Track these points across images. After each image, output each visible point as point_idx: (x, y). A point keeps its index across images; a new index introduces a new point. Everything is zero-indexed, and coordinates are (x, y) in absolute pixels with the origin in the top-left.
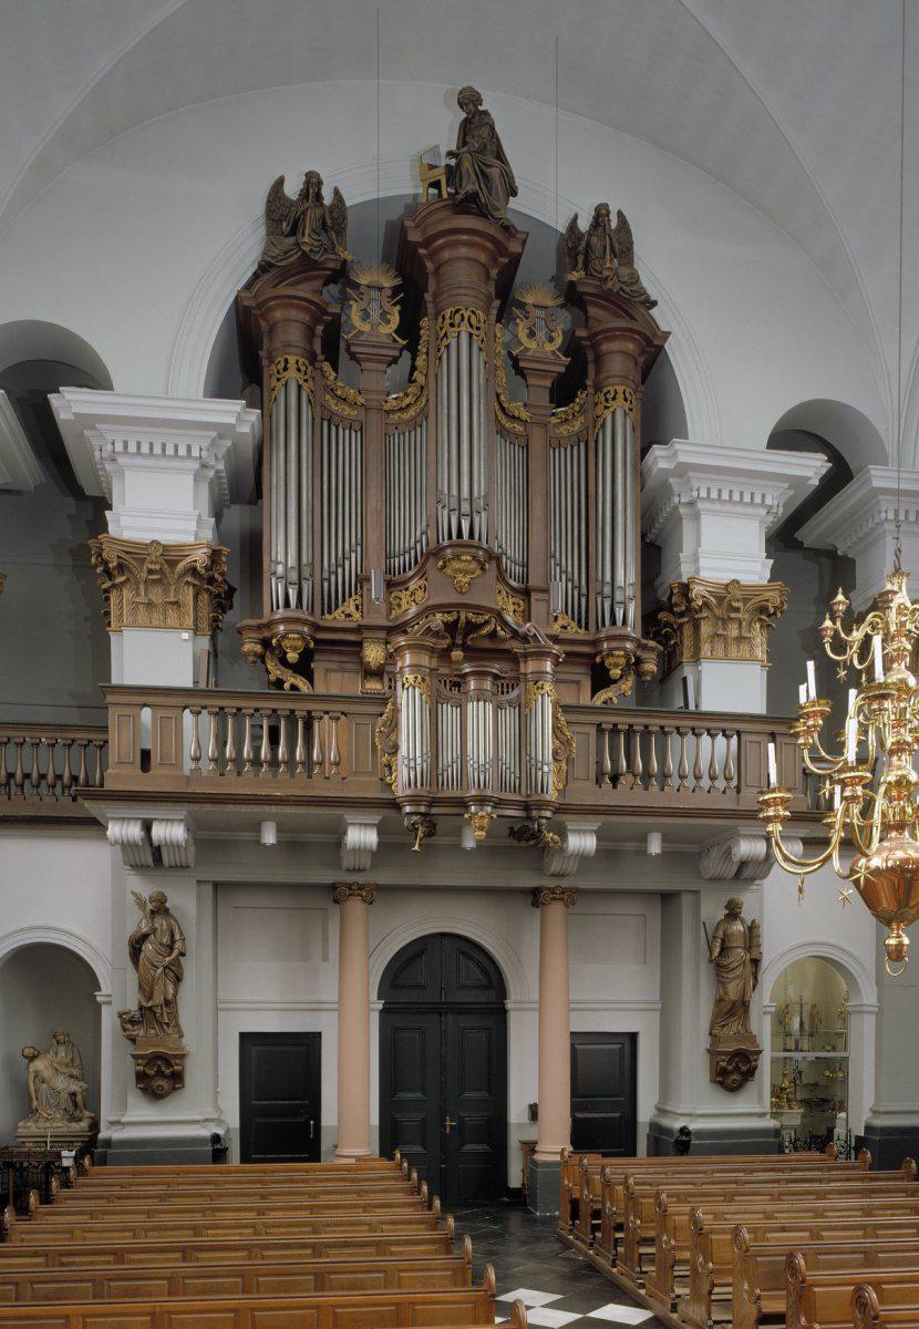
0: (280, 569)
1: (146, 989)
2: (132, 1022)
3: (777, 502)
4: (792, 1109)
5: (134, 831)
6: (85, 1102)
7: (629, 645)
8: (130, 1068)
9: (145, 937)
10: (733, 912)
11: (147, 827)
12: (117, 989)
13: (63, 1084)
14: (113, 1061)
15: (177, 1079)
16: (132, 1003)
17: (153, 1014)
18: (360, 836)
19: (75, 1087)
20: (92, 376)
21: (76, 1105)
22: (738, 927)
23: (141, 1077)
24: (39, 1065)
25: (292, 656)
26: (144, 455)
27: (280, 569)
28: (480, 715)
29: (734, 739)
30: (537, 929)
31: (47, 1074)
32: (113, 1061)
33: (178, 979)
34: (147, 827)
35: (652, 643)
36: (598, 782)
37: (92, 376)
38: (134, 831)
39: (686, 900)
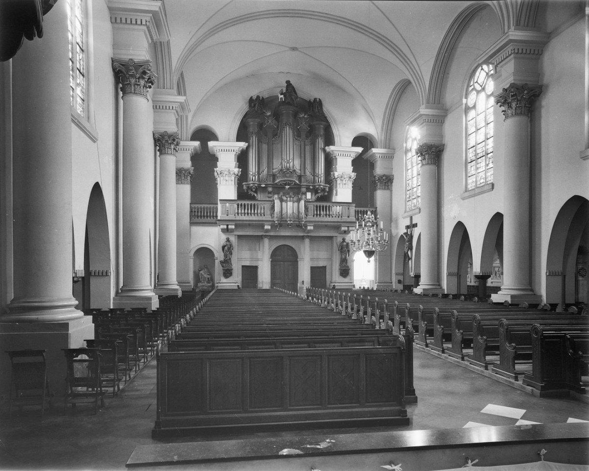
0: (251, 173)
1: (226, 256)
2: (223, 263)
3: (353, 156)
4: (518, 381)
5: (225, 227)
6: (211, 280)
7: (322, 186)
8: (222, 272)
9: (225, 246)
10: (344, 240)
11: (227, 226)
12: (219, 256)
13: (206, 276)
14: (218, 269)
15: (231, 274)
16: (222, 258)
17: (226, 262)
18: (267, 227)
19: (209, 276)
20: (215, 138)
21: (209, 280)
22: (345, 244)
23: (224, 273)
24: (201, 272)
25: (254, 190)
26: (133, 24)
27: (251, 173)
28: (290, 204)
29: (341, 207)
30: (516, 288)
31: (203, 274)
32: (218, 269)
33: (231, 254)
34: (227, 226)
35: (327, 185)
36: (314, 216)
37: (215, 138)
38: (225, 227)
39: (334, 238)
